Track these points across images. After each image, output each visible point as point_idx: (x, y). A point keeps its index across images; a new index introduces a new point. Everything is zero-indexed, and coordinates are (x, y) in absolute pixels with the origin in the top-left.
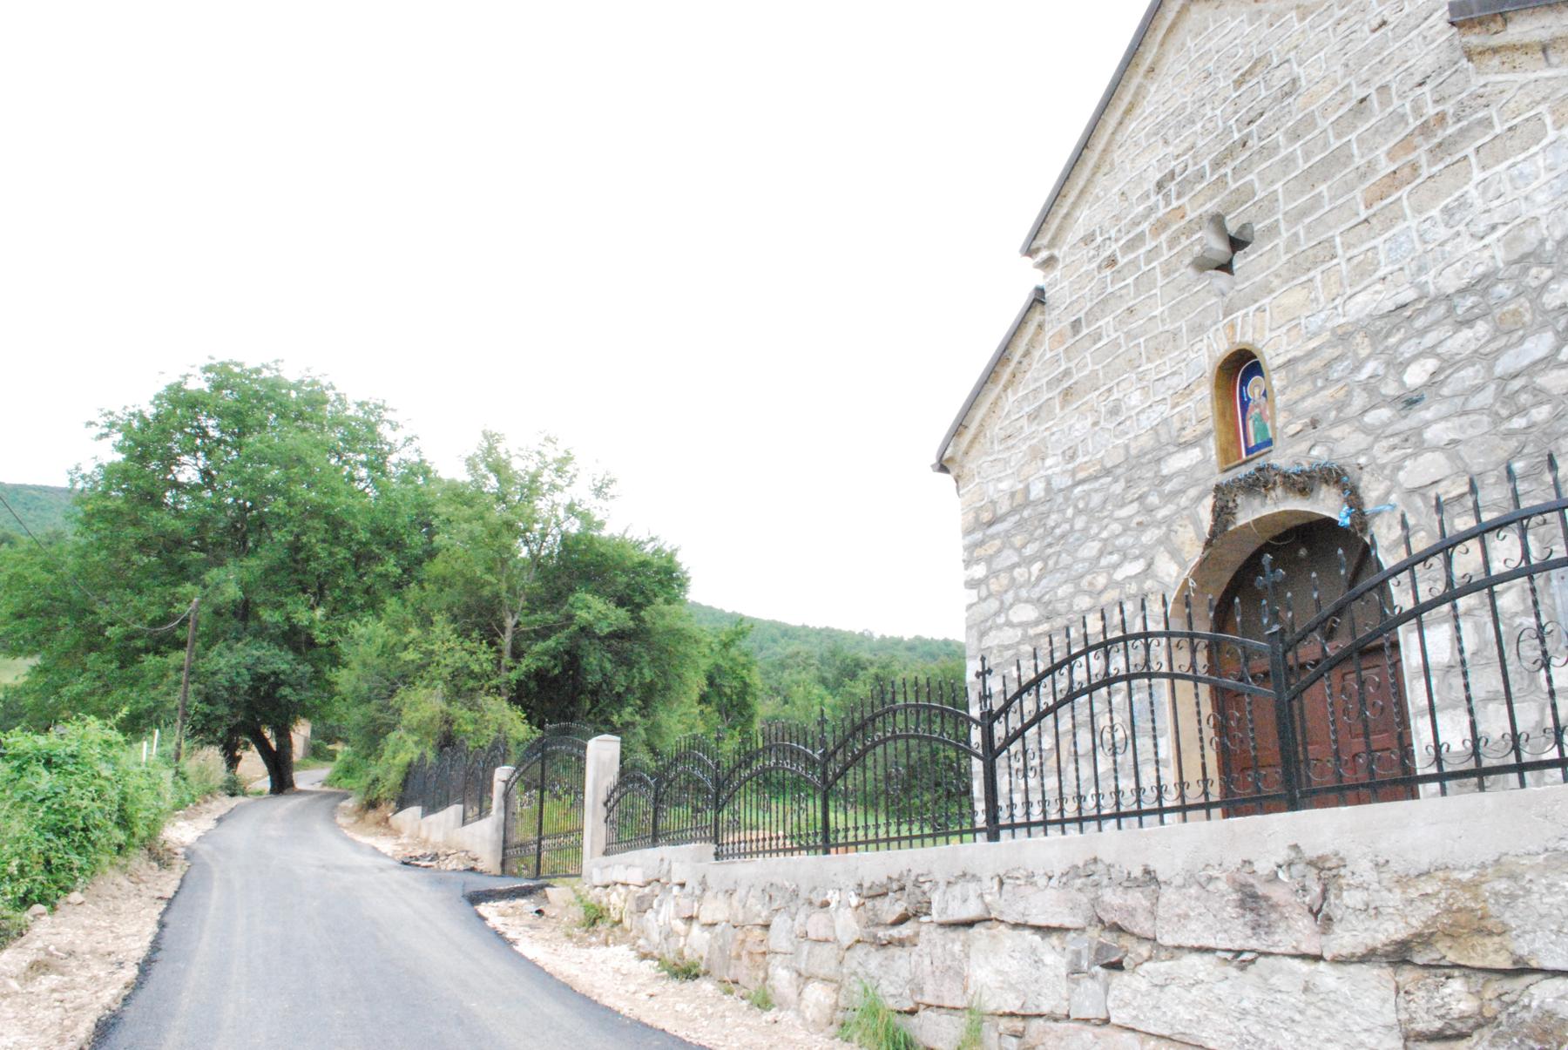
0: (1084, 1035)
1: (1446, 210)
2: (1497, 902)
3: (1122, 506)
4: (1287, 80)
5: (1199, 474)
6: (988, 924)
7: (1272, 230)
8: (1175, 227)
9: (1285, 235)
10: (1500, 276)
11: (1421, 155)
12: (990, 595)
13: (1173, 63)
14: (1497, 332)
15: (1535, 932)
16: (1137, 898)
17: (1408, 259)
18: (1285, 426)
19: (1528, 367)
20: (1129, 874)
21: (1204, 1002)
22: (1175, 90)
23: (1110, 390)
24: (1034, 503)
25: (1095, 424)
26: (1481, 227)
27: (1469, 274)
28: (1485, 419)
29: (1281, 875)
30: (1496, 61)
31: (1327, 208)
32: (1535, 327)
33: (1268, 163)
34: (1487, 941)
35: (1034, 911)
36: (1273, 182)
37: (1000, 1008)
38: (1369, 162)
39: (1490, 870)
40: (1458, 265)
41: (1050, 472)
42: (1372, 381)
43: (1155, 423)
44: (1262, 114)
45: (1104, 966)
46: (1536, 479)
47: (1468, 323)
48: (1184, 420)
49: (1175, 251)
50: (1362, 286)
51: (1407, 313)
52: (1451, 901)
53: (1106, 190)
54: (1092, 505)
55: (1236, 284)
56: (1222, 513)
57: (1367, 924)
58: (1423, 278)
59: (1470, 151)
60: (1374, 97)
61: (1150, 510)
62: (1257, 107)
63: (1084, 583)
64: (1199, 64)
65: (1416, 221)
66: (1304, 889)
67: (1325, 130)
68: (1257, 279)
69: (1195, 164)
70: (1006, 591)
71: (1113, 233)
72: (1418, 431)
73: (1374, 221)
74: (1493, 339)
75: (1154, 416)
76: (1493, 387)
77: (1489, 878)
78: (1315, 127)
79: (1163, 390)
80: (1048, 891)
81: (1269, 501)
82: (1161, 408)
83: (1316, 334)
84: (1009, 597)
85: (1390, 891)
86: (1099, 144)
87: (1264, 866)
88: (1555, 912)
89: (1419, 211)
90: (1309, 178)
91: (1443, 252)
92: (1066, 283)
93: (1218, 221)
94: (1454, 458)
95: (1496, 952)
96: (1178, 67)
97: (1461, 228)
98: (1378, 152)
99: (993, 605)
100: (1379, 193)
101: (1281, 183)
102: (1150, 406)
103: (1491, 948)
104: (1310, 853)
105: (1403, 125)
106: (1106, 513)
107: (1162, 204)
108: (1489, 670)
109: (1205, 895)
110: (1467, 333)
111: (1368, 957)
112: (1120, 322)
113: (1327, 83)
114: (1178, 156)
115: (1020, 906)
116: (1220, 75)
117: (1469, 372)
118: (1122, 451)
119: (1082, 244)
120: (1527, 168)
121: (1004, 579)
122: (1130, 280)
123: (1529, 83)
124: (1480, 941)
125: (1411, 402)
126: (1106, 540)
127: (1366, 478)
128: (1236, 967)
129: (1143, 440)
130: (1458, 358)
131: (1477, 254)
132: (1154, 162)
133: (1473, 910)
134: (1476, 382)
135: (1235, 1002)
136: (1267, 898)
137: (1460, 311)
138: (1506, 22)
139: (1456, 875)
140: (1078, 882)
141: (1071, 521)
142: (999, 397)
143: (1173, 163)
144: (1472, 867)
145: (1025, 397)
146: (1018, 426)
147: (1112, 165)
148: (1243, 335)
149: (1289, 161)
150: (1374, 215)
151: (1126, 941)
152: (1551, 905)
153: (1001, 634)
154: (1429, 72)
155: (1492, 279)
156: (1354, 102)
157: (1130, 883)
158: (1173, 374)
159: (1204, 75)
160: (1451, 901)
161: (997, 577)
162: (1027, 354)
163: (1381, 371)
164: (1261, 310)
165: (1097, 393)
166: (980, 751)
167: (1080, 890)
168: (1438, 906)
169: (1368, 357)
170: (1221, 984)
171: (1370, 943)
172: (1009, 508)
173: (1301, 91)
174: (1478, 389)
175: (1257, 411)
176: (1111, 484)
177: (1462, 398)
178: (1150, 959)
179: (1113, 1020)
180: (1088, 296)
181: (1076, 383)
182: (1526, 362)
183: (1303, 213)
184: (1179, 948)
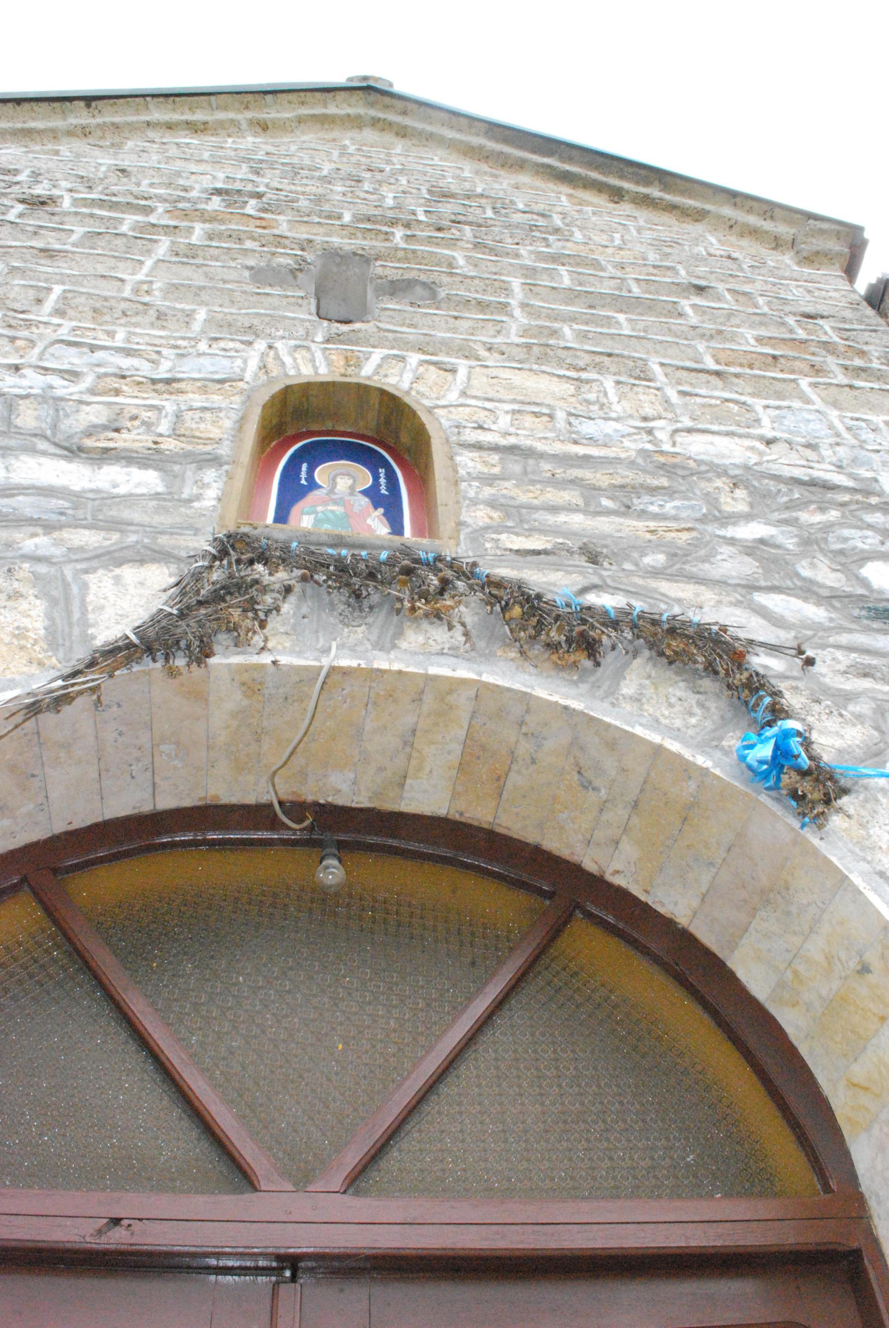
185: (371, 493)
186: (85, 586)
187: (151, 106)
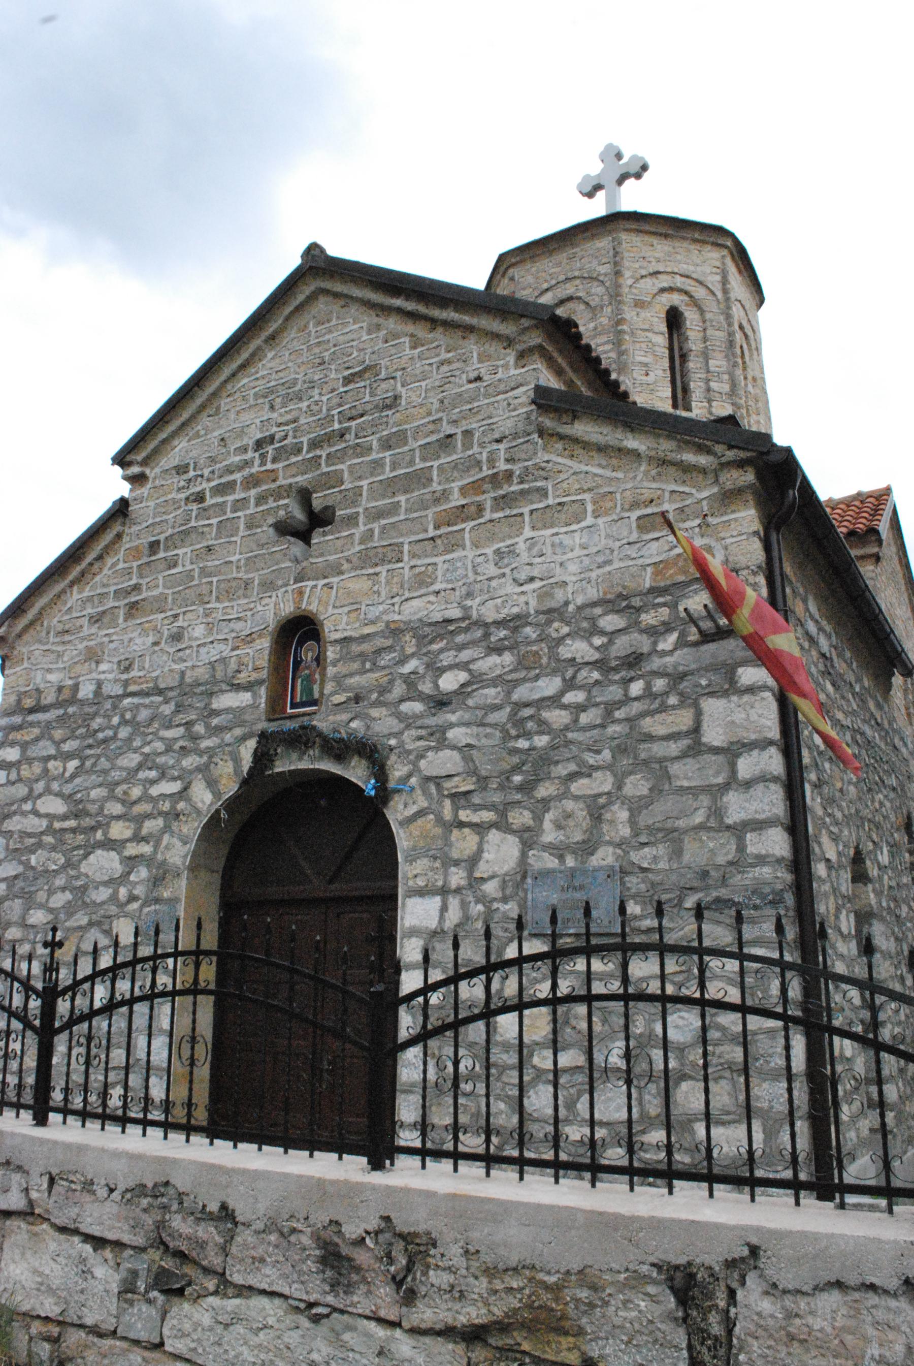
0: (132, 1356)
1: (498, 552)
2: (577, 1308)
3: (169, 727)
4: (390, 394)
5: (247, 717)
6: (31, 1219)
7: (352, 520)
8: (264, 487)
9: (362, 528)
10: (529, 620)
11: (487, 499)
12: (20, 780)
13: (292, 339)
14: (521, 664)
15: (607, 1339)
16: (208, 1232)
17: (461, 583)
20: (204, 1206)
21: (272, 1348)
22: (290, 364)
23: (176, 616)
24: (82, 703)
25: (156, 644)
26: (523, 577)
27: (506, 611)
28: (498, 733)
29: (368, 1241)
30: (559, 446)
31: (402, 517)
32: (548, 670)
33: (359, 460)
34: (562, 1339)
35: (89, 1219)
36: (360, 478)
37: (33, 1309)
38: (445, 490)
39: (573, 1278)
40: (499, 601)
41: (102, 677)
42: (412, 676)
44: (362, 415)
45: (162, 1292)
47: (498, 650)
48: (240, 664)
49: (261, 508)
51: (451, 628)
52: (534, 1298)
53: (207, 431)
54: (138, 719)
55: (311, 556)
56: (262, 758)
57: (450, 1305)
58: (469, 603)
59: (526, 510)
60: (459, 437)
61: (195, 738)
62: (359, 407)
63: (119, 790)
64: (317, 350)
65: (473, 553)
66: (389, 1255)
67: (413, 450)
68: (331, 558)
69: (295, 437)
70: (37, 780)
71: (206, 472)
72: (443, 730)
73: (439, 542)
76: (508, 709)
77: (571, 1284)
78: (406, 444)
79: (226, 631)
80: (108, 1204)
81: (306, 757)
82: (222, 647)
83: (373, 622)
84: (40, 787)
85: (476, 1278)
86: (211, 387)
87: (352, 1230)
88: (628, 1325)
90: (391, 486)
91: (489, 586)
92: (152, 504)
93: (305, 496)
94: (467, 759)
95: (569, 1349)
96: (296, 345)
97: (507, 571)
98: (453, 485)
99: (21, 790)
102: (212, 642)
103: (565, 1346)
104: (401, 1227)
106: (150, 730)
107: (257, 462)
109: (285, 1244)
110: (494, 659)
111: (447, 1332)
112: (197, 557)
114: (280, 425)
115: (74, 1212)
116: (333, 367)
117: (491, 691)
118: (177, 677)
119: (174, 472)
120: (567, 540)
121: (37, 768)
122: (214, 521)
124: (556, 1338)
125: (441, 702)
126: (148, 755)
127: (393, 758)
128: (310, 1319)
129: (200, 671)
130: (485, 677)
131: (515, 597)
132: (258, 421)
133: (552, 1310)
135: (305, 1352)
136: (349, 1259)
137: (493, 639)
139: (541, 1276)
140: (145, 1202)
141: (116, 729)
142: (64, 591)
143: (275, 429)
144: (558, 1272)
145: (90, 599)
146: (78, 624)
147: (218, 408)
148: (309, 603)
149: (378, 464)
150: (440, 536)
151: (188, 1270)
152: (625, 1319)
153: (25, 821)
154: (507, 433)
156: (442, 435)
157: (203, 1215)
158: (239, 619)
159: (318, 361)
160: (534, 1298)
161: (30, 764)
162: (100, 558)
163: (421, 670)
164: (329, 586)
165: (163, 615)
166: (37, 1023)
167: (145, 1210)
168: (521, 1300)
169: (413, 655)
170: (291, 1333)
171: (450, 1321)
172: (54, 700)
173: (399, 408)
174: (496, 708)
175: (307, 672)
176: (161, 703)
178: (216, 1293)
179: (168, 1348)
180: (171, 523)
181: (143, 600)
182: (537, 696)
183: (380, 514)
184: (250, 1288)
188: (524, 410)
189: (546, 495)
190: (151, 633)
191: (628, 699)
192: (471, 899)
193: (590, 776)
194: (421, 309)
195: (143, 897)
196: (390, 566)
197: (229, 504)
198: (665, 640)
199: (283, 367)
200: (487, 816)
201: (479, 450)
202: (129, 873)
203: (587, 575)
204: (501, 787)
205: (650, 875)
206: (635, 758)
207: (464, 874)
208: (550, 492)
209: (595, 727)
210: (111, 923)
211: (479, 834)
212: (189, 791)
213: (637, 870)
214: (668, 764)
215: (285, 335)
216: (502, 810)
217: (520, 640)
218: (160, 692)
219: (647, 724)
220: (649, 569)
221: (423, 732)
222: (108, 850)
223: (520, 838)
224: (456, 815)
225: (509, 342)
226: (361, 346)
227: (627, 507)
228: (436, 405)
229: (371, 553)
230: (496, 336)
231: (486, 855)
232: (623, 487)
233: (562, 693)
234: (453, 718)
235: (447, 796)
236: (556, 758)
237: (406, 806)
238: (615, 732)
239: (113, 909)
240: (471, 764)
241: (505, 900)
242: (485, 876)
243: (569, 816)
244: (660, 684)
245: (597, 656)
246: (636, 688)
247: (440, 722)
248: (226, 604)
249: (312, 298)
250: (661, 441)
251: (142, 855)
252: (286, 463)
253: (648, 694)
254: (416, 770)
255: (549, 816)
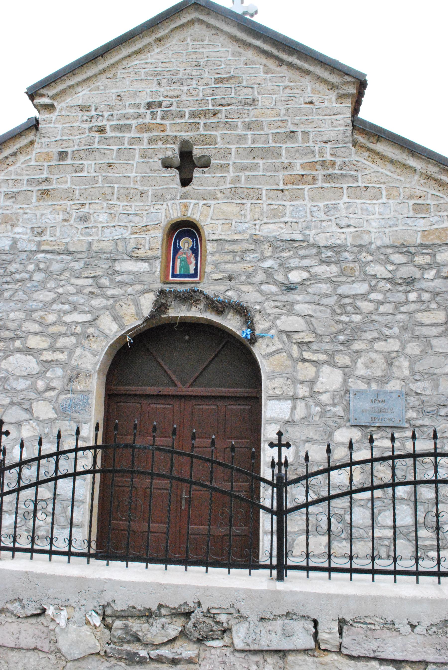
5: (145, 278)
7: (223, 168)
14: (342, 273)
17: (302, 220)
18: (212, 273)
19: (354, 295)
23: (82, 205)
26: (344, 222)
27: (333, 241)
28: (329, 311)
30: (366, 154)
31: (261, 173)
33: (229, 132)
40: (328, 234)
41: (18, 236)
42: (270, 270)
43: (117, 237)
44: (229, 105)
46: (347, 346)
50: (274, 221)
54: (52, 269)
58: (307, 232)
59: (345, 186)
61: (101, 287)
62: (227, 99)
63: (36, 315)
65: (310, 204)
72: (292, 304)
73: (286, 192)
74: (339, 276)
75: (115, 233)
78: (262, 129)
89: (312, 199)
91: (321, 225)
92: (60, 126)
97: (333, 218)
100: (292, 180)
101: (235, 146)
105: (312, 156)
108: (310, 428)
110: (324, 268)
113: (274, 112)
117: (323, 286)
120: (370, 208)
123: (378, 172)
130: (319, 277)
131: (338, 234)
132: (148, 90)
134: (327, 292)
137: (323, 256)
138: (378, 141)
147: (115, 75)
150: (287, 190)
154: (331, 139)
155: (343, 248)
156: (288, 130)
158: (136, 215)
163: (276, 267)
165: (71, 202)
174: (327, 296)
175: (185, 256)
177: (319, 297)
181: (54, 190)
182: (353, 293)
183: (244, 168)
185: (192, 249)
186: (140, 300)
187: (122, 48)
188: (342, 128)
189: (357, 180)
190: (61, 213)
191: (407, 302)
192: (311, 403)
193: (386, 340)
194: (274, 51)
195: (59, 388)
196: (253, 201)
197: (126, 139)
198: (429, 273)
199: (168, 60)
200: (322, 357)
201: (313, 145)
202: (45, 372)
203: (383, 229)
204: (332, 341)
205: (422, 397)
206: (412, 333)
207: (308, 389)
208: (360, 179)
209: (389, 314)
210: (31, 404)
211: (316, 367)
212: (98, 322)
213: (414, 394)
214: (431, 339)
215: (169, 40)
216: (332, 355)
217: (341, 259)
218: (70, 253)
219: (419, 316)
220: (420, 234)
221: (279, 304)
222: (26, 354)
223: (343, 371)
224: (301, 354)
225: (333, 87)
226: (228, 62)
227: (406, 197)
228: (283, 111)
229: (239, 191)
230: (325, 81)
231: (321, 379)
232: (404, 185)
233: (369, 293)
234: (299, 298)
235: (294, 343)
236: (366, 329)
237: (268, 346)
238: (401, 318)
239: (32, 395)
240: (311, 326)
241: (334, 405)
242: (321, 391)
243: (373, 362)
244: (426, 296)
245: (390, 276)
246: (412, 296)
247: (289, 300)
248: (126, 204)
249: (192, 22)
250: (430, 166)
251: (57, 360)
252: (172, 122)
253: (419, 300)
254: (274, 325)
255: (360, 361)
